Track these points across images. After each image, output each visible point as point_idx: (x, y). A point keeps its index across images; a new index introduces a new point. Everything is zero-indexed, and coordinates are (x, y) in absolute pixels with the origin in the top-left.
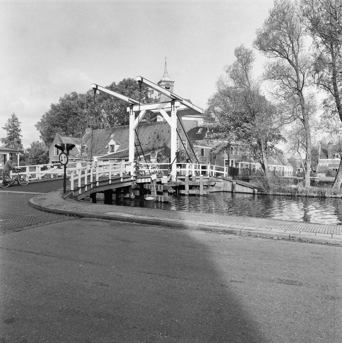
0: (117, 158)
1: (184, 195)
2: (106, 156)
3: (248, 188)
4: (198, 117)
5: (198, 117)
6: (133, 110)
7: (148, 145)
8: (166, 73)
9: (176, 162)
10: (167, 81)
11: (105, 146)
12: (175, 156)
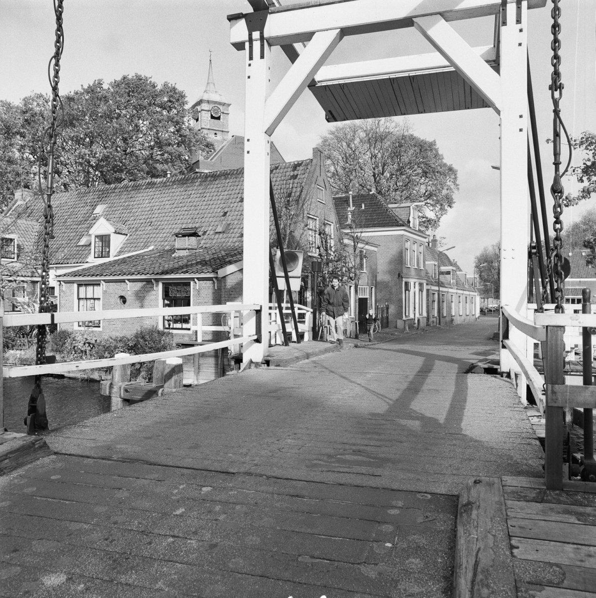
6: (266, 35)
7: (225, 235)
8: (212, 85)
10: (215, 103)
11: (79, 239)
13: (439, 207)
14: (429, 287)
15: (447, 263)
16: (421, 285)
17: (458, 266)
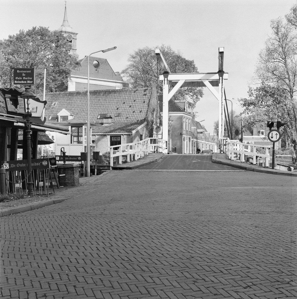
0: (101, 134)
3: (281, 166)
4: (116, 82)
5: (116, 82)
8: (66, 22)
10: (69, 33)
13: (196, 97)
14: (193, 139)
15: (200, 127)
16: (189, 138)
17: (205, 129)
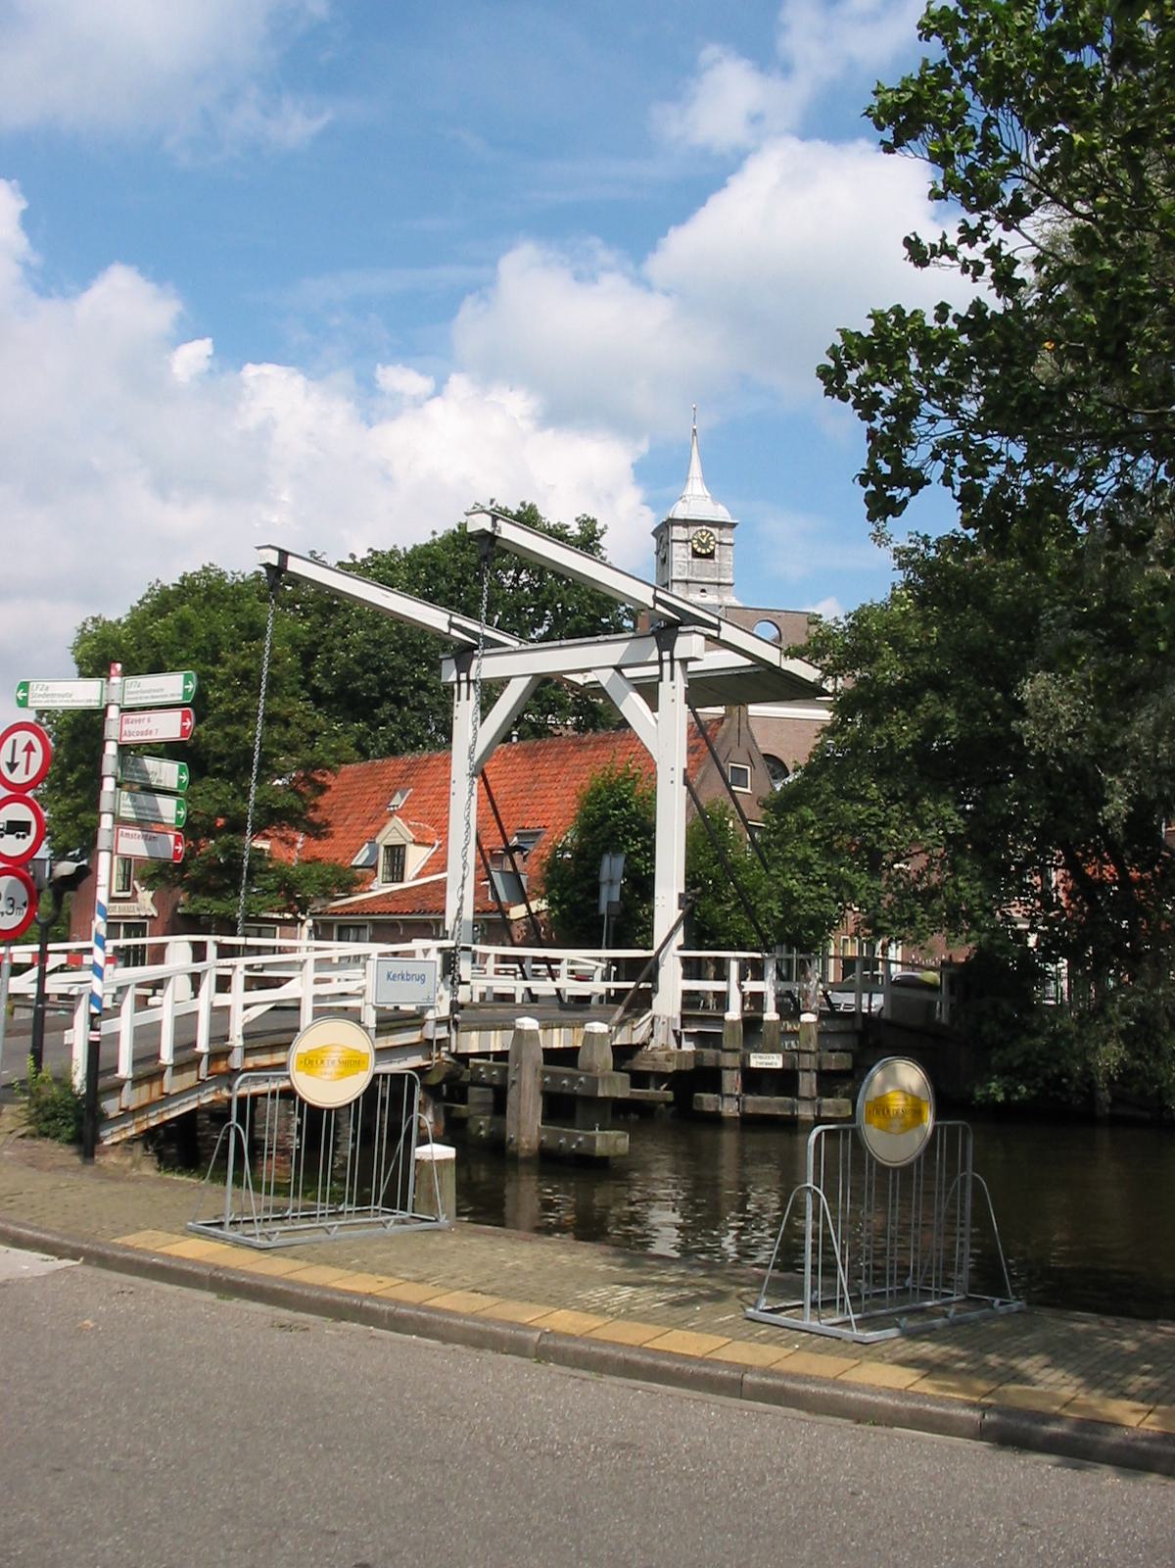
1: (716, 1120)
2: (362, 902)
6: (675, 657)
9: (680, 948)
12: (676, 913)
15: (508, 942)
